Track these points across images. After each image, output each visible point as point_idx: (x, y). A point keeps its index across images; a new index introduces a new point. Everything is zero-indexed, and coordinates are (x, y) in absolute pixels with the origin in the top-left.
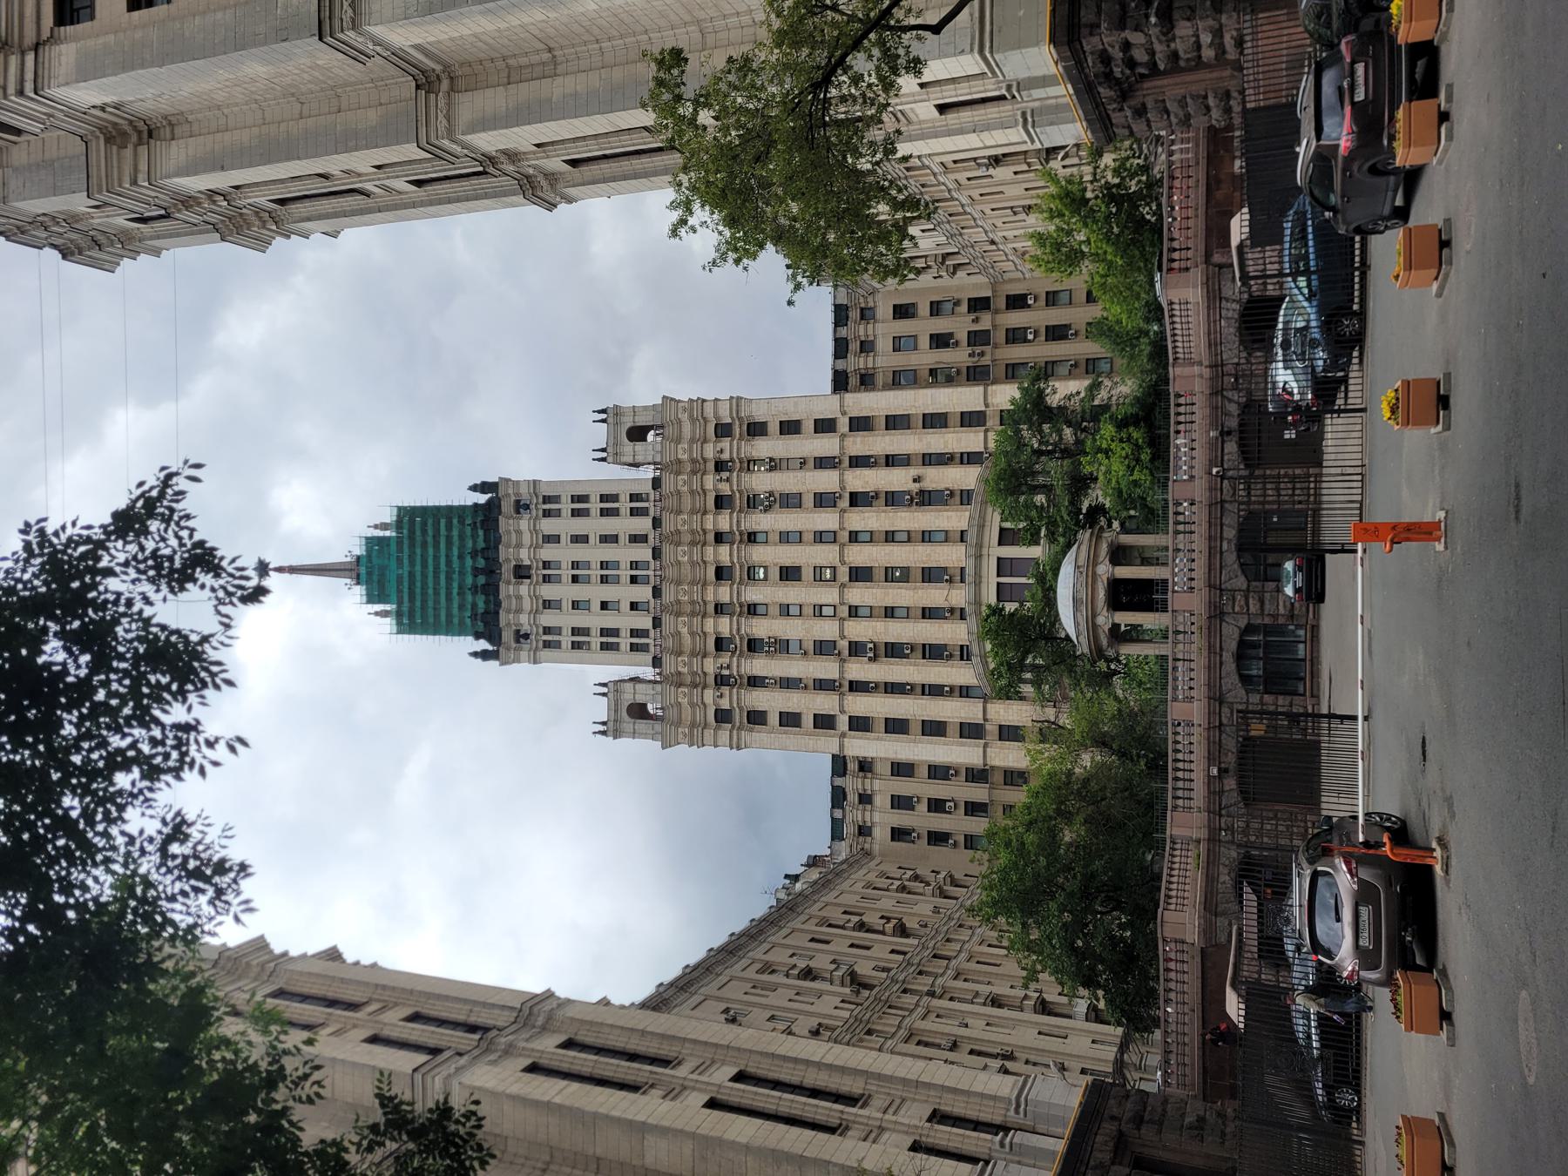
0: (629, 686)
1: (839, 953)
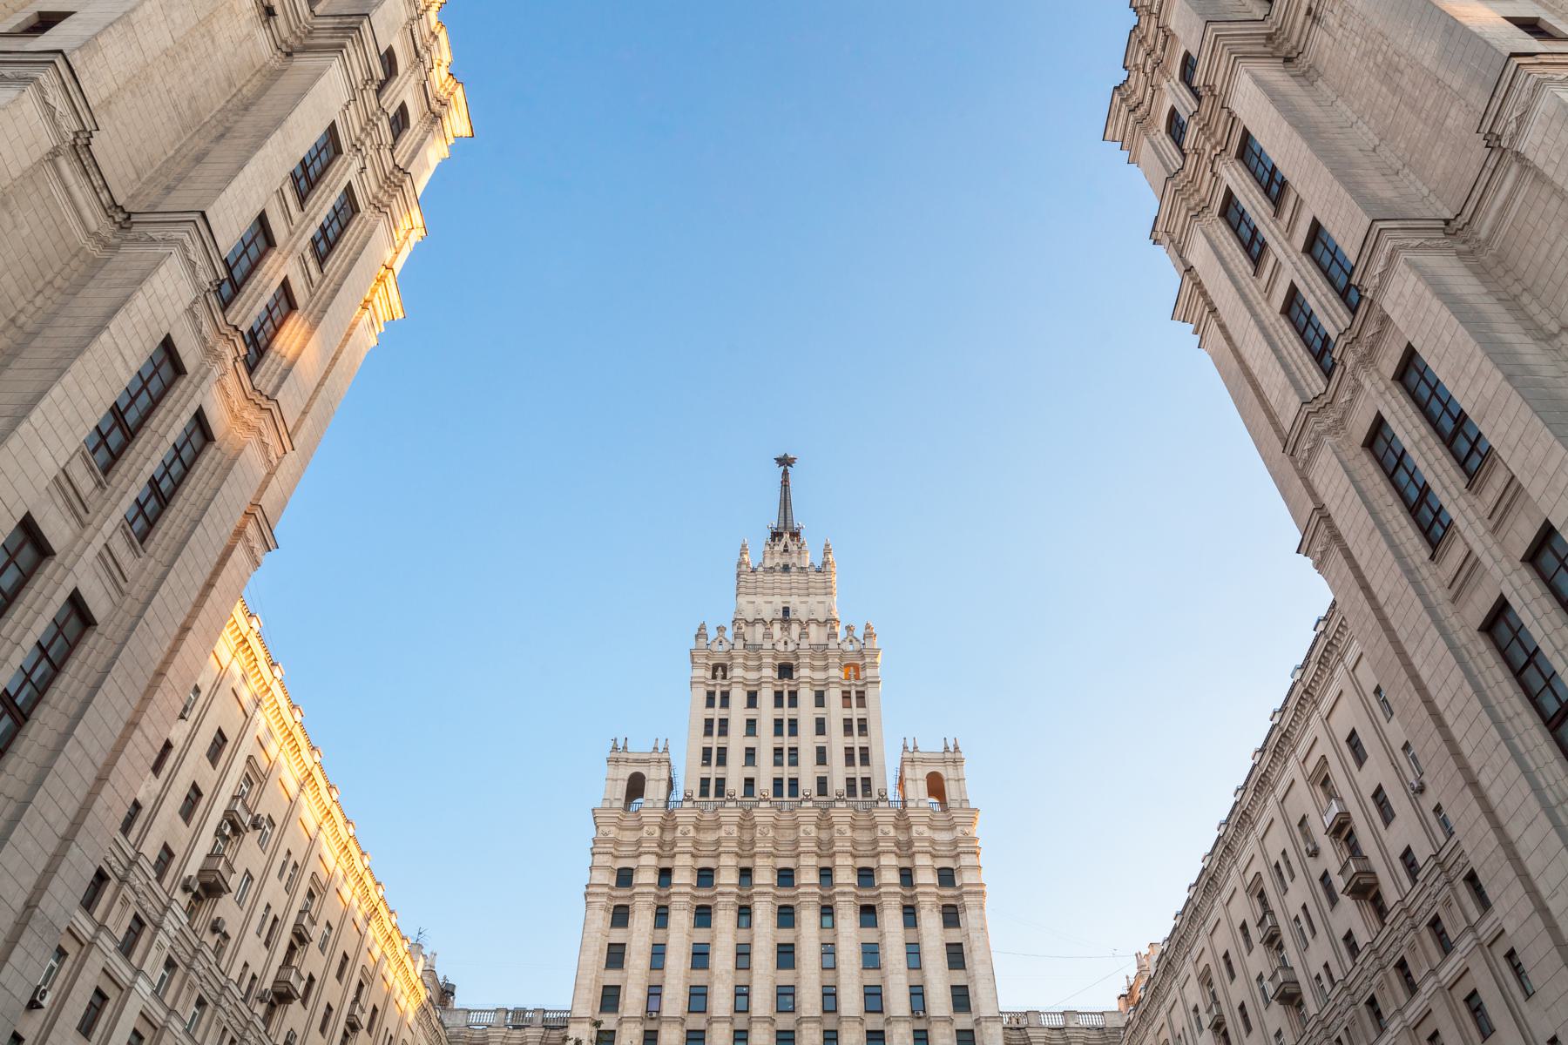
0: (665, 775)
1: (321, 988)
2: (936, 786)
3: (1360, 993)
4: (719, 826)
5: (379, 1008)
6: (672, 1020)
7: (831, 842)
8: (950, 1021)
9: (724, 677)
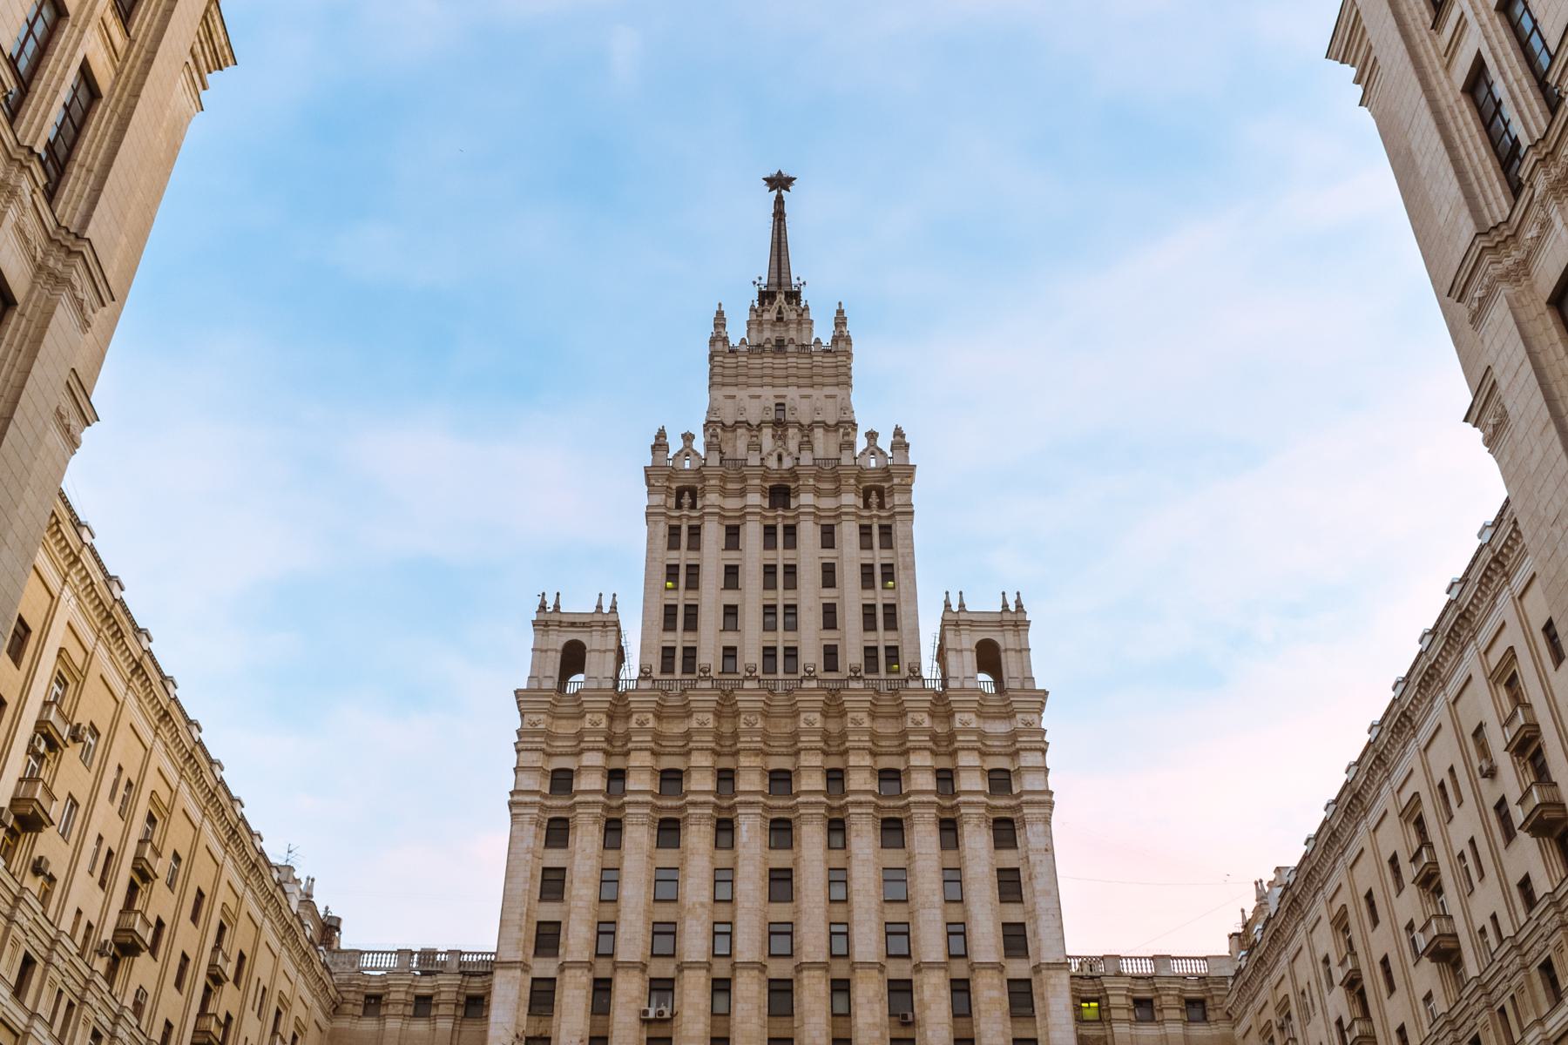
0: (612, 644)
1: (173, 934)
2: (988, 657)
3: (1533, 954)
4: (689, 714)
5: (247, 954)
6: (630, 966)
7: (843, 736)
8: (1000, 968)
9: (693, 506)
